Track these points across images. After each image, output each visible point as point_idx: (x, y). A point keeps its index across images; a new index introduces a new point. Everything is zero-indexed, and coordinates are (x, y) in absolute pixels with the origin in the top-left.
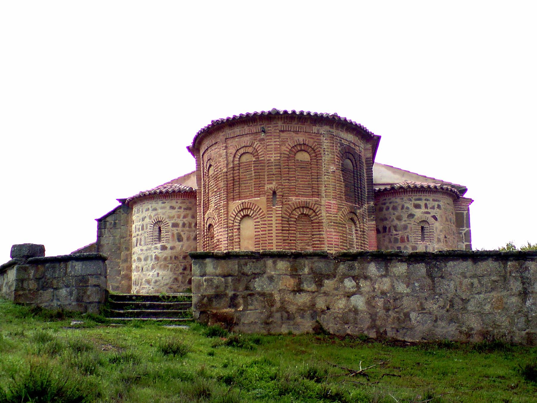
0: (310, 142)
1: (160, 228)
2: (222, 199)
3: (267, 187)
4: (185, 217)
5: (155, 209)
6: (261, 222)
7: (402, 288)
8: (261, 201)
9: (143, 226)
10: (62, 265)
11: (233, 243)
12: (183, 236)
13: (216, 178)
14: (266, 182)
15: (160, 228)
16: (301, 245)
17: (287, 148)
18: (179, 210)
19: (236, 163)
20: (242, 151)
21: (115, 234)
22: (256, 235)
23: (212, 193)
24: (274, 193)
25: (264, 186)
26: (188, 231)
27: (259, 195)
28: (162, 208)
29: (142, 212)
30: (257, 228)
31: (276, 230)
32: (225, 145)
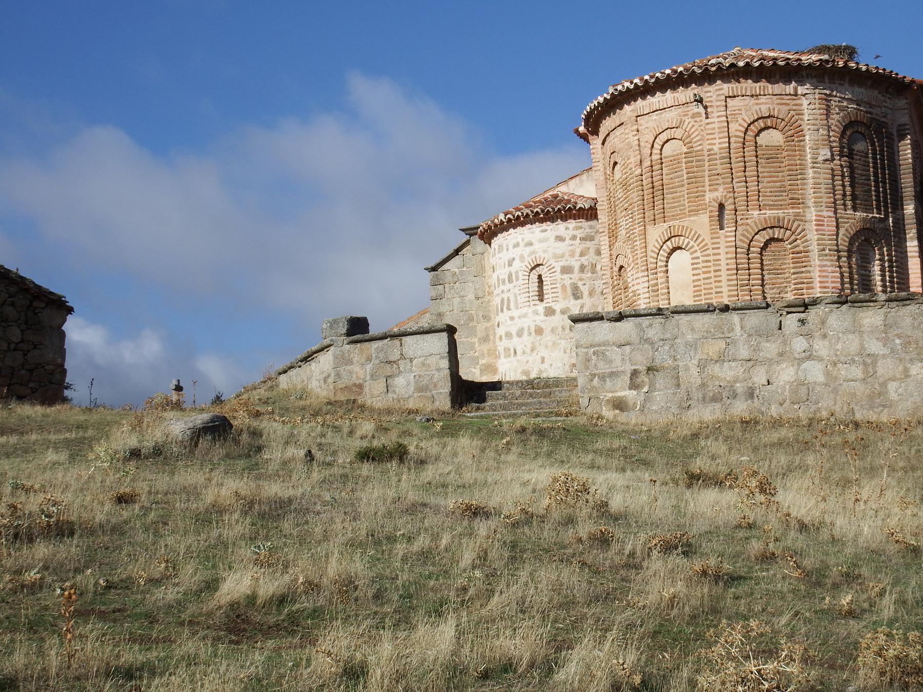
0: (780, 110)
1: (540, 277)
2: (637, 222)
3: (709, 196)
4: (582, 254)
5: (530, 244)
6: (702, 258)
7: (875, 347)
8: (702, 223)
9: (510, 275)
10: (396, 342)
11: (658, 295)
12: (582, 288)
13: (625, 185)
14: (707, 188)
15: (540, 277)
16: (771, 292)
17: (740, 125)
18: (572, 242)
19: (655, 157)
20: (663, 137)
21: (462, 293)
22: (694, 281)
23: (621, 212)
24: (721, 207)
25: (704, 196)
26: (590, 279)
27: (694, 212)
28: (541, 241)
29: (507, 250)
30: (696, 269)
31: (728, 270)
32: (635, 127)
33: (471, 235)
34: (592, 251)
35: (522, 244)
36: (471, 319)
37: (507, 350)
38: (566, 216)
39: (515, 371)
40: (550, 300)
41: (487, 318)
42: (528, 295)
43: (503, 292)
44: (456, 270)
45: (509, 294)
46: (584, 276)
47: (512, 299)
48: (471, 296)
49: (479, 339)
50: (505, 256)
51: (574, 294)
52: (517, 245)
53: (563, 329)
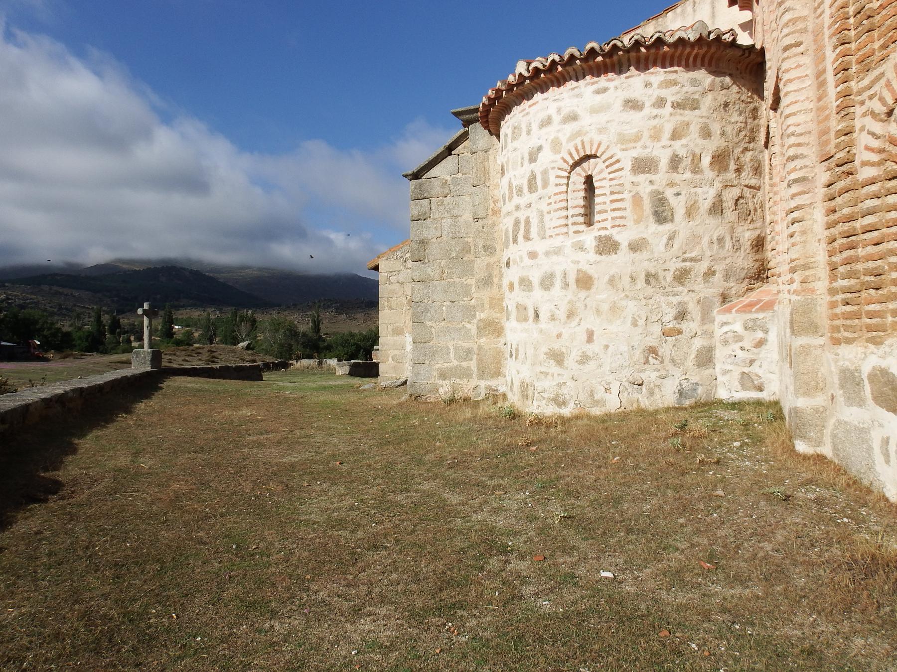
1: (589, 180)
4: (676, 135)
5: (573, 117)
9: (532, 179)
12: (673, 201)
15: (589, 180)
18: (656, 111)
21: (455, 212)
26: (688, 183)
28: (594, 111)
33: (467, 123)
34: (694, 129)
35: (556, 119)
36: (466, 249)
37: (521, 308)
38: (647, 59)
39: (536, 349)
40: (608, 224)
41: (489, 249)
42: (564, 213)
43: (518, 208)
44: (448, 178)
45: (528, 213)
46: (677, 177)
47: (534, 221)
48: (467, 216)
49: (478, 281)
50: (524, 144)
51: (656, 213)
52: (547, 122)
53: (633, 279)
